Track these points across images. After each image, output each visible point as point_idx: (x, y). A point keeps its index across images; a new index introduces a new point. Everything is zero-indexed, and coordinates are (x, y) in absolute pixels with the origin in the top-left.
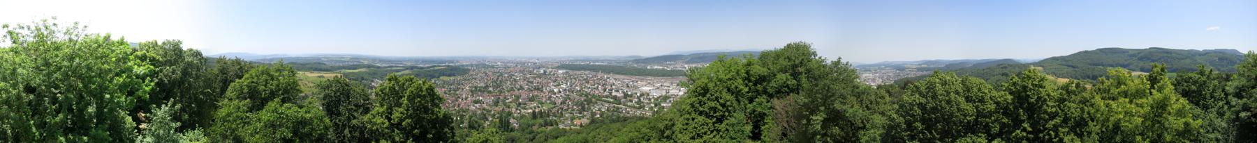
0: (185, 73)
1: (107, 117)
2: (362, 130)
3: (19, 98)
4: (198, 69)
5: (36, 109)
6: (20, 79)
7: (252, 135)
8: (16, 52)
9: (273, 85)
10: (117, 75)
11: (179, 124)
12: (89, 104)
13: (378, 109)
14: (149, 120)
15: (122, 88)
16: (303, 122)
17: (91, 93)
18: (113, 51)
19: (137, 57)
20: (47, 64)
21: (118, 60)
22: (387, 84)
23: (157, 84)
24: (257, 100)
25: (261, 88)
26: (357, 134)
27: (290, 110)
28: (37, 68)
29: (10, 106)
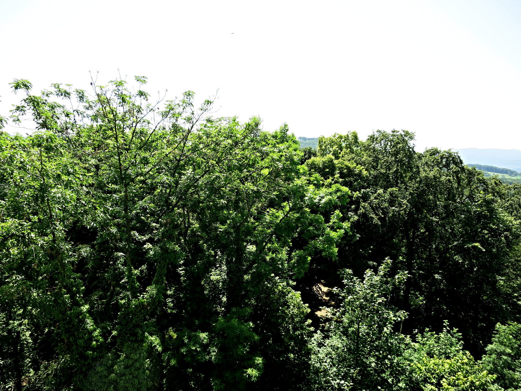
0: (419, 202)
1: (250, 291)
3: (53, 253)
4: (451, 196)
5: (97, 277)
6: (56, 211)
8: (49, 149)
10: (272, 204)
11: (402, 314)
12: (211, 264)
14: (336, 301)
15: (282, 231)
17: (218, 242)
18: (264, 155)
19: (313, 167)
20: (123, 178)
21: (275, 174)
23: (355, 226)
28: (100, 186)
29: (30, 275)
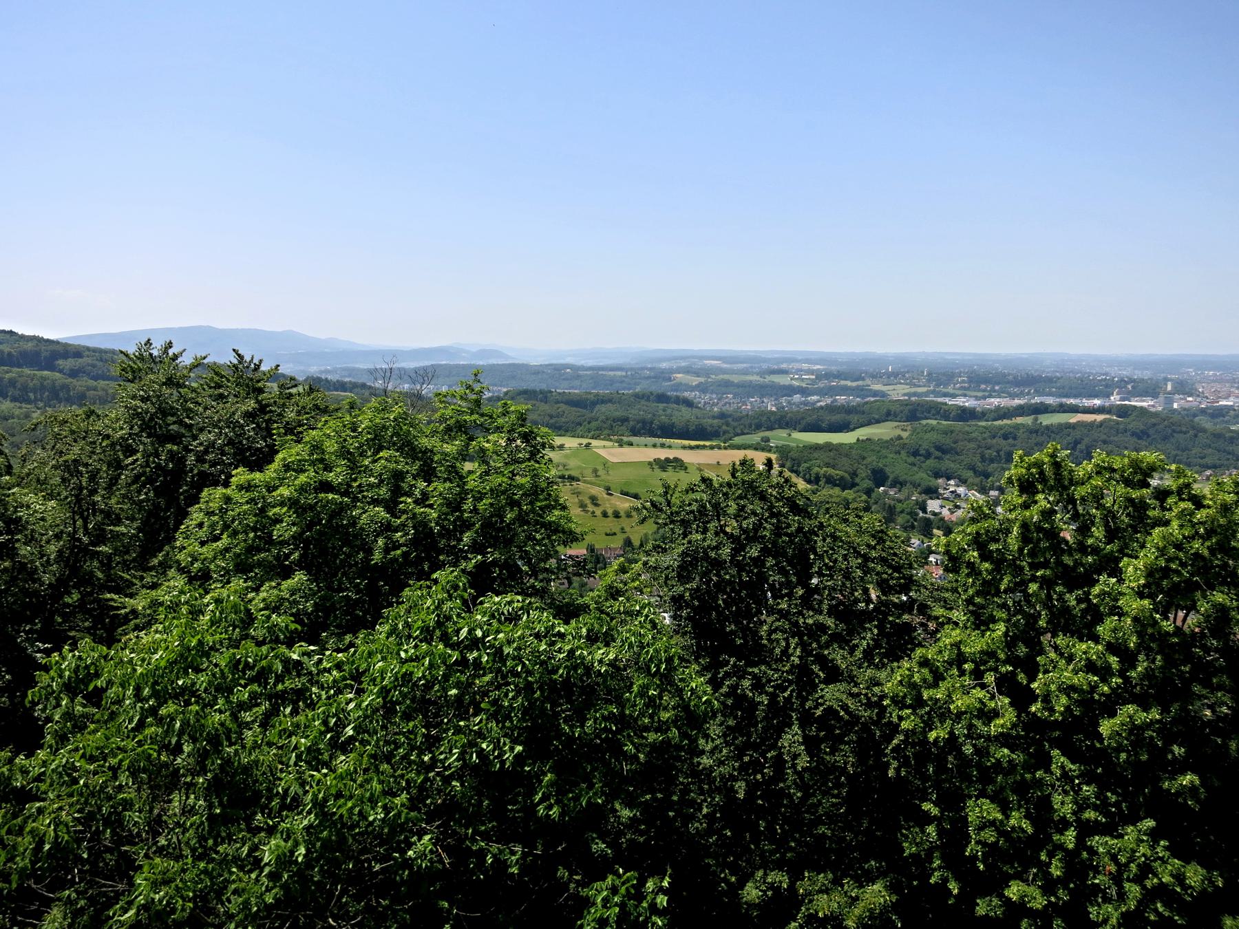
2: (870, 735)
7: (314, 759)
9: (429, 503)
13: (956, 635)
16: (579, 689)
22: (1009, 508)
24: (345, 574)
25: (370, 515)
26: (845, 758)
27: (513, 626)
